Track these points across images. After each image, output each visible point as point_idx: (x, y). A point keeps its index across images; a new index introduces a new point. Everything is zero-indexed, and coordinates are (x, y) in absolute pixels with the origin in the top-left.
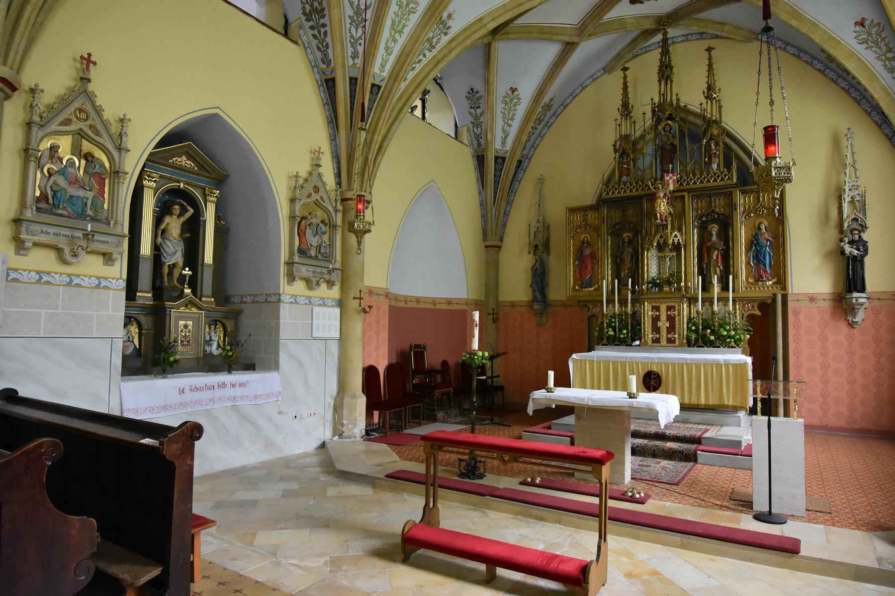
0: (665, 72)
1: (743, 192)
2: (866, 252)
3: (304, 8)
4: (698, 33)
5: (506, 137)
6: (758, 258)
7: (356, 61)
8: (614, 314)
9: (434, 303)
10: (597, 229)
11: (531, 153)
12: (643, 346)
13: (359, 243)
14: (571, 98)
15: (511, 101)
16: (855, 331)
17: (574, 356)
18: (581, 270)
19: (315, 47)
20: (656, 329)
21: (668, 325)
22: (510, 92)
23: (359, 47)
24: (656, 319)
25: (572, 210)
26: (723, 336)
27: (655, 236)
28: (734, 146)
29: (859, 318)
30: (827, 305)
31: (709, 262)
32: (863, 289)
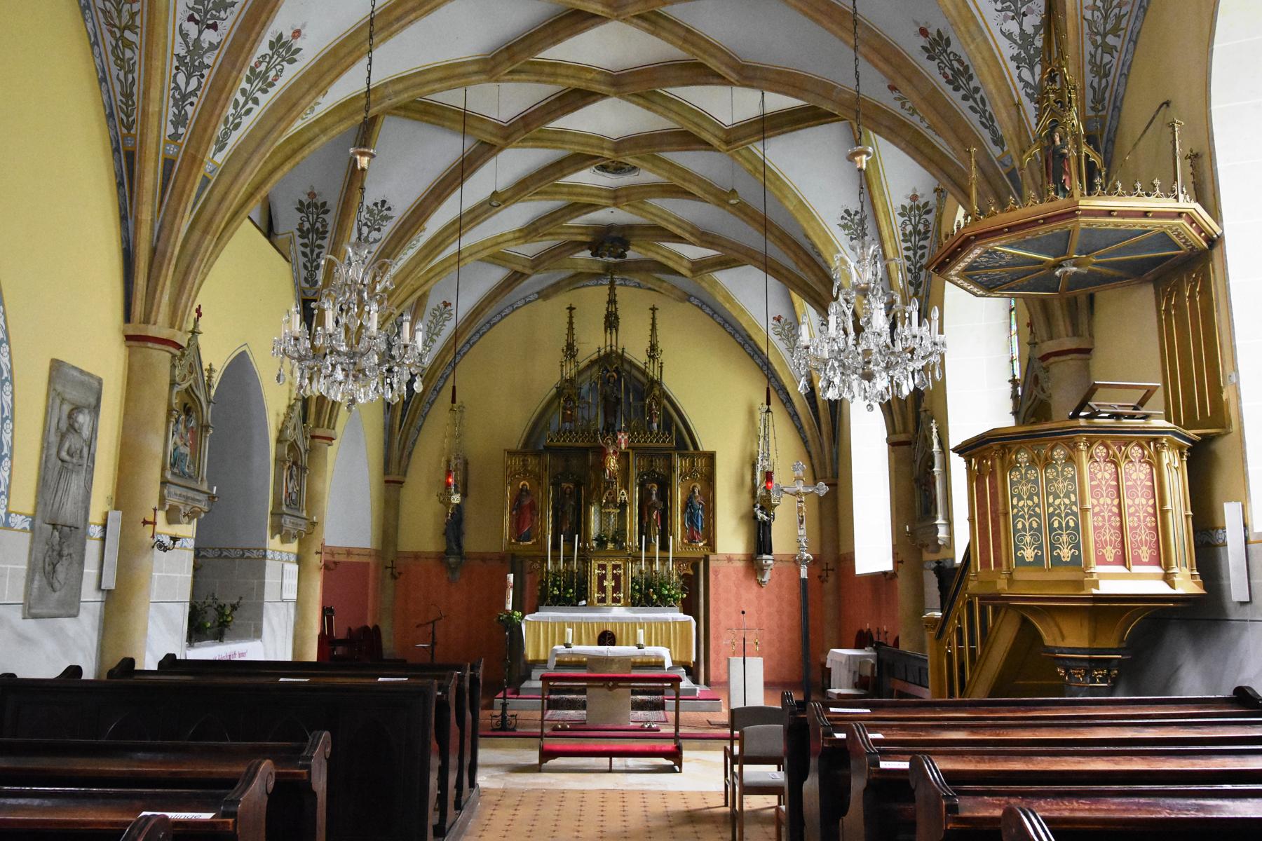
0: (612, 322)
1: (682, 456)
3: (301, 225)
6: (691, 519)
9: (333, 555)
10: (539, 479)
12: (590, 606)
15: (441, 315)
16: (763, 590)
18: (518, 523)
19: (301, 264)
20: (602, 589)
22: (442, 306)
23: (188, 108)
28: (674, 414)
30: (740, 565)
32: (770, 553)
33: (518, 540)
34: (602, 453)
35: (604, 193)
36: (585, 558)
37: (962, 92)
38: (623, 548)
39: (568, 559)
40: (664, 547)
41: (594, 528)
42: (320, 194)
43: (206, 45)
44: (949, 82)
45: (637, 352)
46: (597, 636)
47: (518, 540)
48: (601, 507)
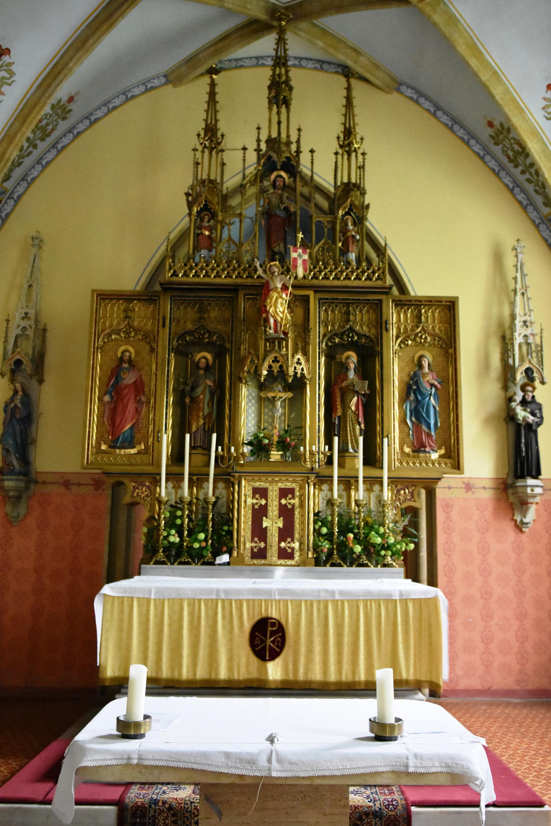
0: (280, 94)
4: (318, 61)
6: (418, 413)
8: (181, 500)
10: (150, 339)
11: (20, 190)
14: (105, 109)
16: (524, 537)
17: (107, 589)
20: (259, 533)
21: (281, 525)
24: (260, 513)
25: (103, 297)
26: (374, 545)
27: (265, 357)
29: (531, 516)
31: (344, 414)
32: (537, 474)
33: (113, 446)
34: (261, 291)
36: (227, 477)
37: (520, 168)
38: (298, 458)
39: (198, 479)
40: (372, 459)
41: (247, 422)
44: (510, 161)
46: (248, 626)
47: (113, 446)
48: (261, 387)
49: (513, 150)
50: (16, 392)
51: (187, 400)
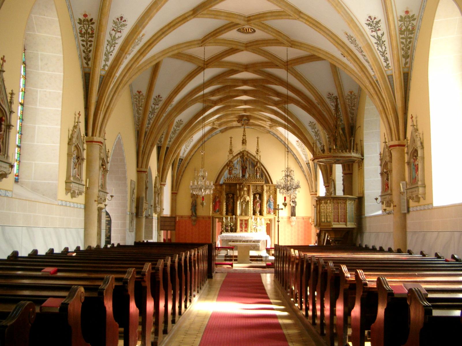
0: (244, 142)
2: (296, 205)
3: (81, 31)
5: (185, 152)
7: (149, 125)
13: (11, 170)
15: (139, 97)
22: (137, 93)
32: (295, 216)
35: (242, 110)
42: (90, 15)
43: (381, 36)
45: (253, 152)
49: (87, 30)
50: (193, 200)
51: (228, 204)
